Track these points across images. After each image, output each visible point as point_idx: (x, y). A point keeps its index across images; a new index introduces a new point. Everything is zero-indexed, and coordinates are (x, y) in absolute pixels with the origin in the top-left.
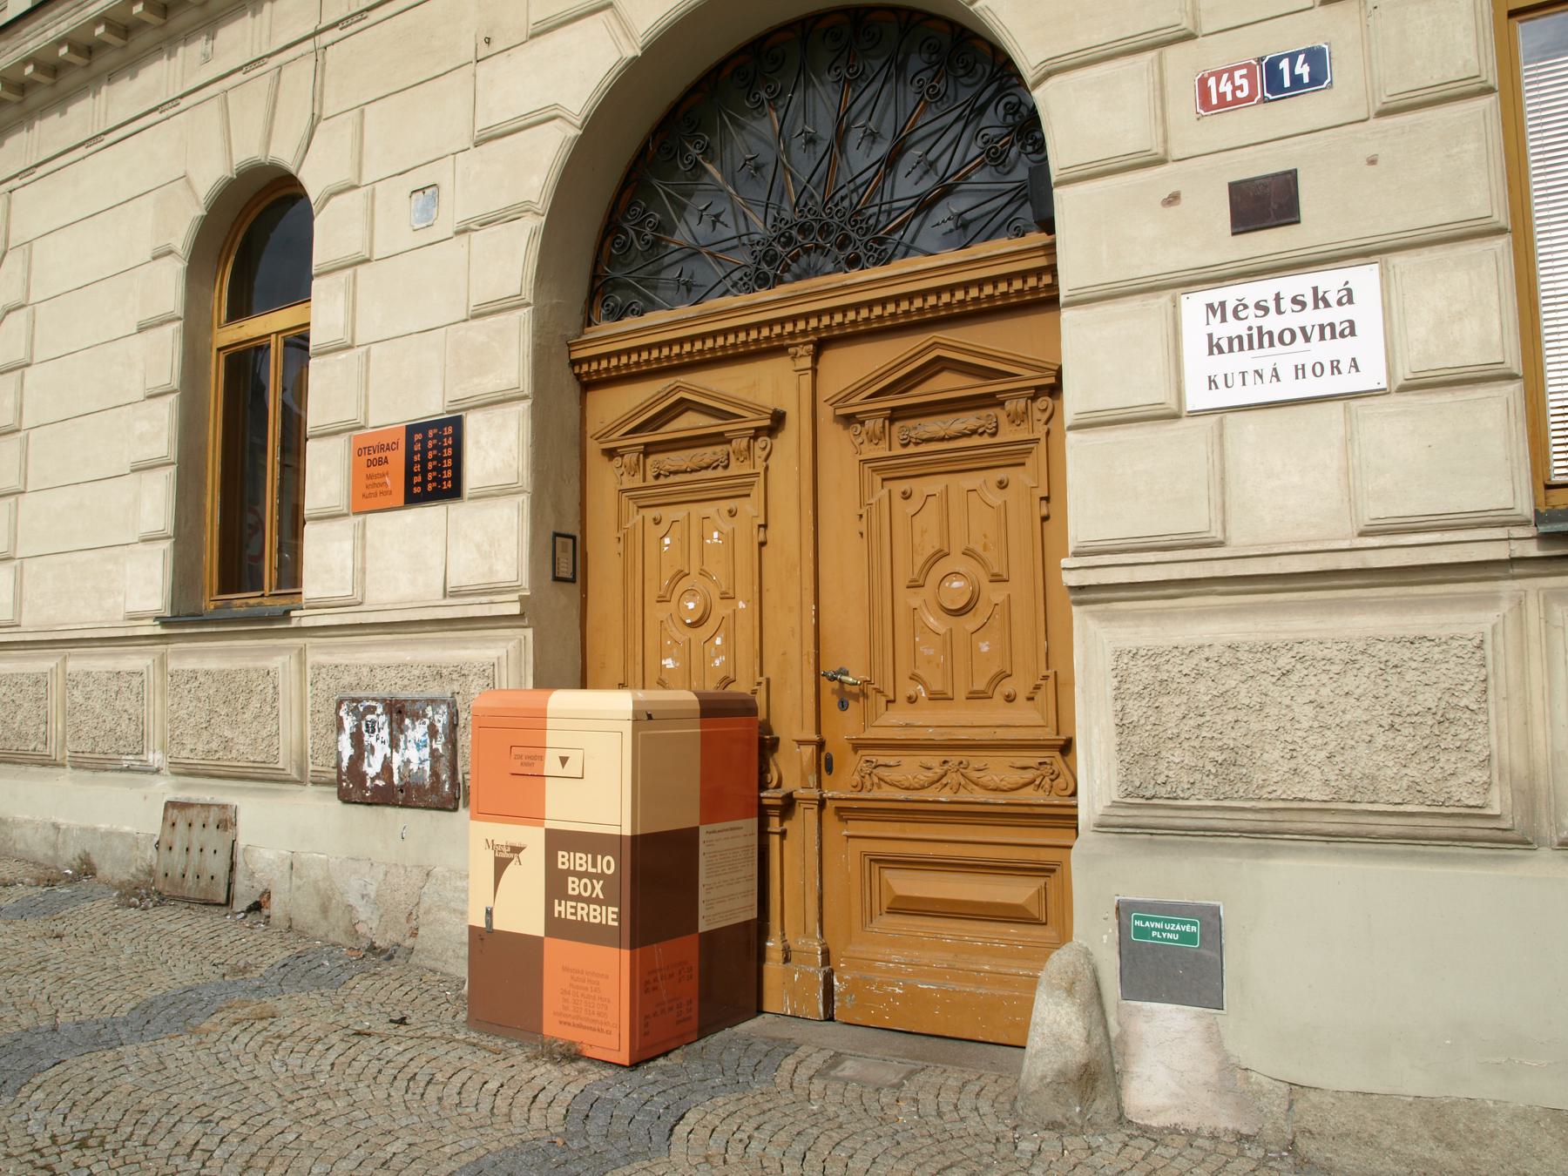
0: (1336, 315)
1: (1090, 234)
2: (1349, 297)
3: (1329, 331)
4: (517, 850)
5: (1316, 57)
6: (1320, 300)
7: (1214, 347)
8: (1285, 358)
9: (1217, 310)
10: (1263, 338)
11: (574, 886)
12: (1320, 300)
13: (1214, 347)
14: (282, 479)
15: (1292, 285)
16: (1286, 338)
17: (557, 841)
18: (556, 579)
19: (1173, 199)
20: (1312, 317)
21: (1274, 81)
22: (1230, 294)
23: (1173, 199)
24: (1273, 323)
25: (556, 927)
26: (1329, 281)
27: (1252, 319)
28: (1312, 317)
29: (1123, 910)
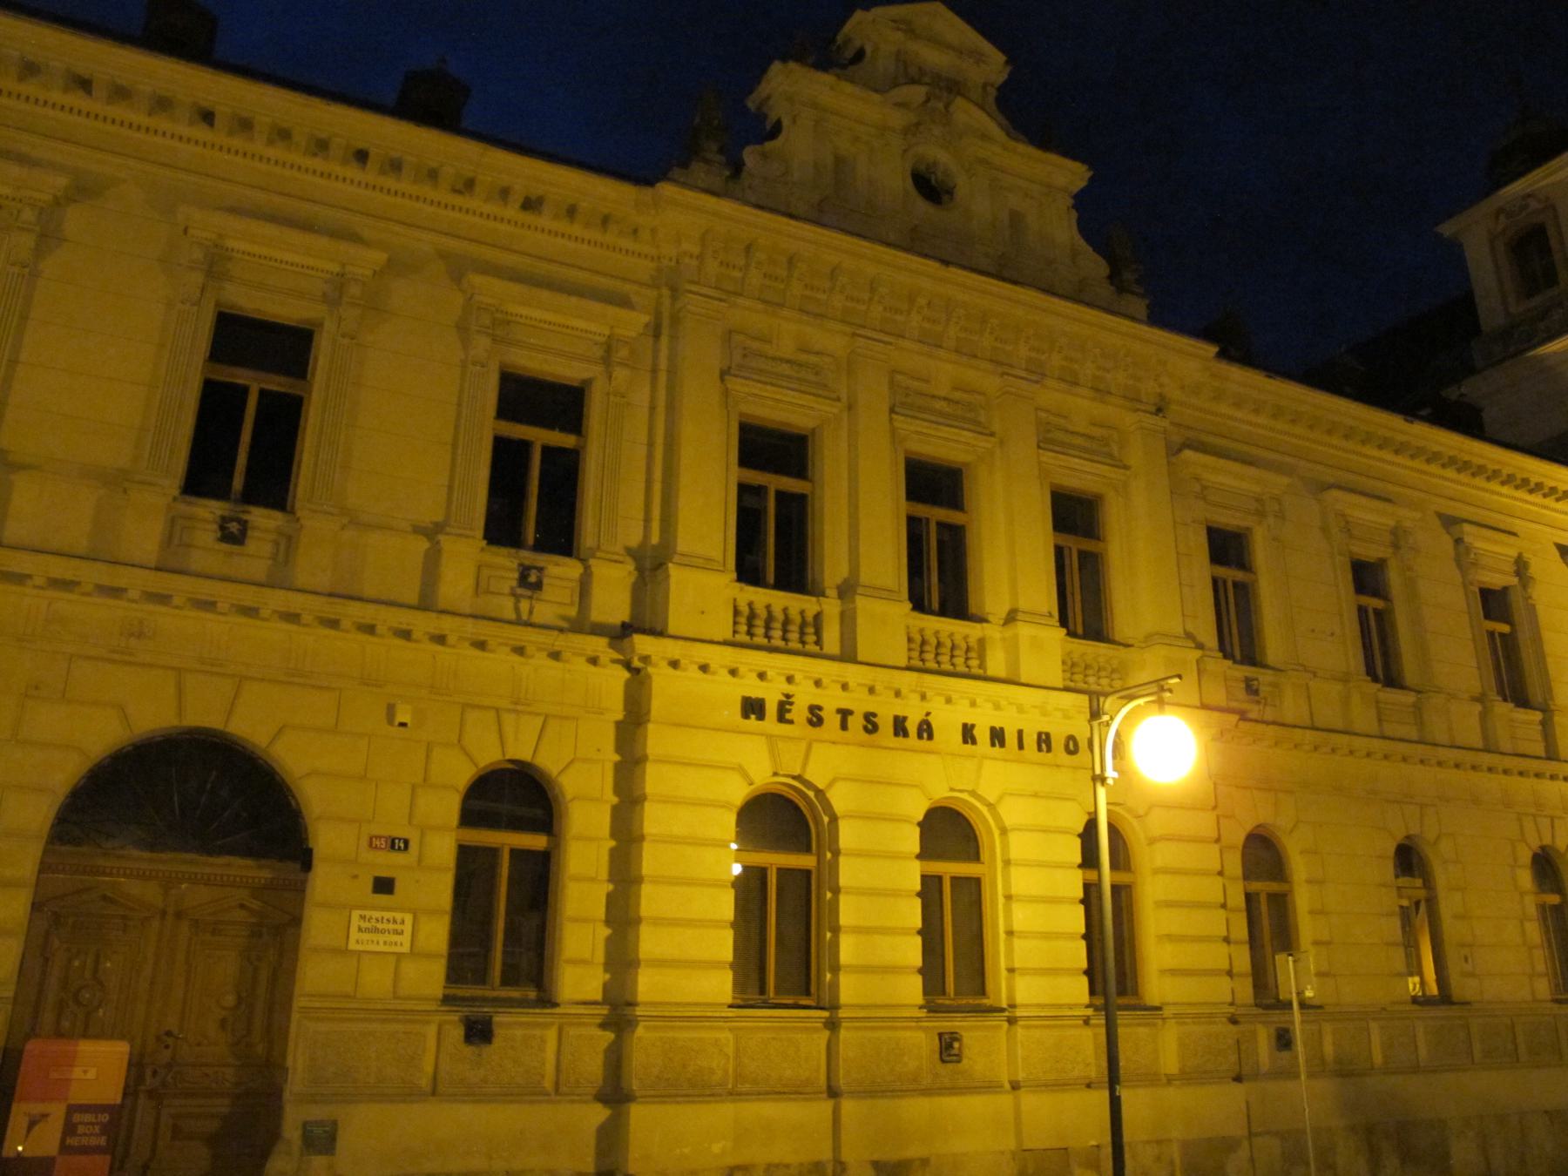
0: (398, 927)
1: (324, 881)
2: (403, 922)
3: (396, 932)
4: (45, 1116)
5: (406, 842)
6: (395, 922)
7: (360, 930)
8: (381, 938)
9: (363, 917)
10: (376, 930)
11: (81, 1129)
12: (395, 922)
13: (360, 930)
14: (1089, 304)
15: (387, 915)
16: (383, 932)
17: (72, 1109)
18: (730, 332)
19: (356, 877)
20: (391, 926)
21: (392, 844)
22: (368, 913)
23: (356, 877)
24: (380, 926)
25: (65, 1149)
26: (399, 916)
27: (373, 923)
28: (391, 926)
29: (305, 1124)
